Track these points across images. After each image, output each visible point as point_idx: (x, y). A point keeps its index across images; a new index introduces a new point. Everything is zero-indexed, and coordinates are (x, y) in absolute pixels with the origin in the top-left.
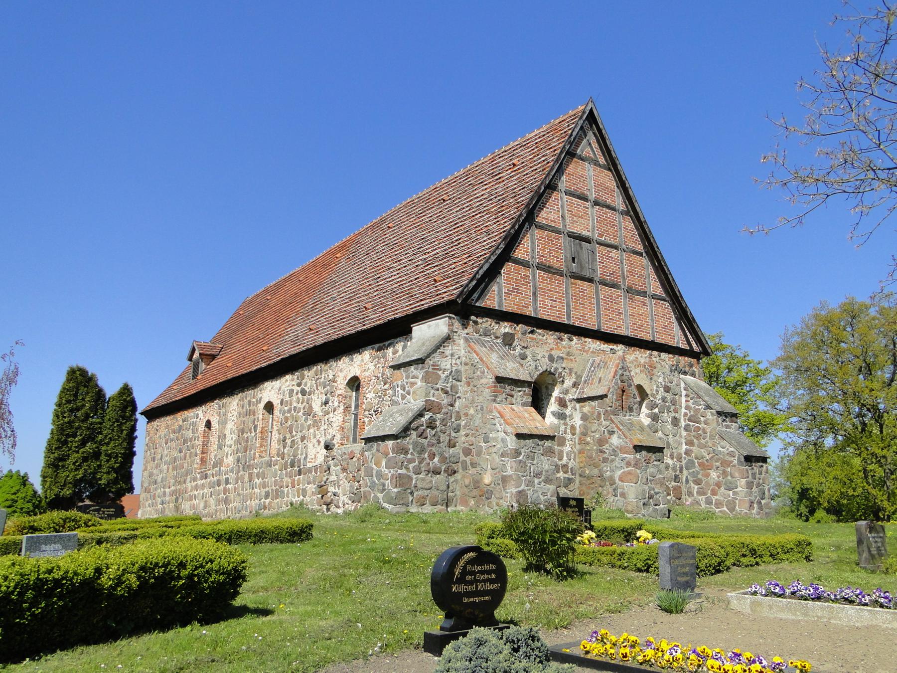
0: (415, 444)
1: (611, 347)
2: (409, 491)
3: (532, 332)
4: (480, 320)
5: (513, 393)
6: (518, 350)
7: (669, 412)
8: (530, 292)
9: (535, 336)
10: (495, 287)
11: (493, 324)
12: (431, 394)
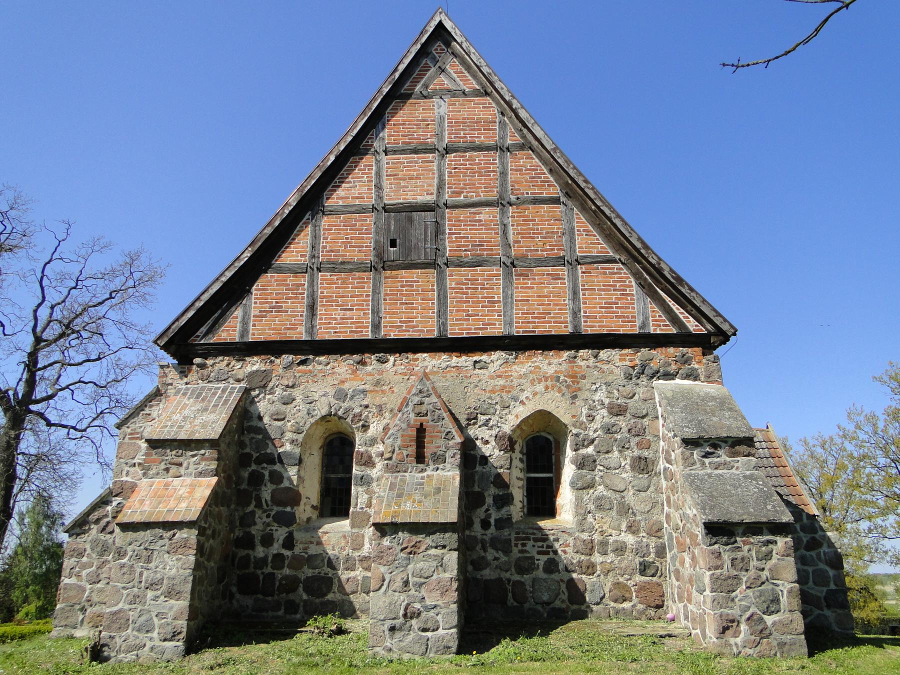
0: (95, 543)
1: (476, 358)
2: (78, 607)
3: (303, 363)
4: (209, 362)
5: (181, 459)
6: (278, 391)
7: (623, 448)
8: (302, 308)
9: (310, 367)
10: (238, 312)
11: (233, 363)
12: (124, 473)
